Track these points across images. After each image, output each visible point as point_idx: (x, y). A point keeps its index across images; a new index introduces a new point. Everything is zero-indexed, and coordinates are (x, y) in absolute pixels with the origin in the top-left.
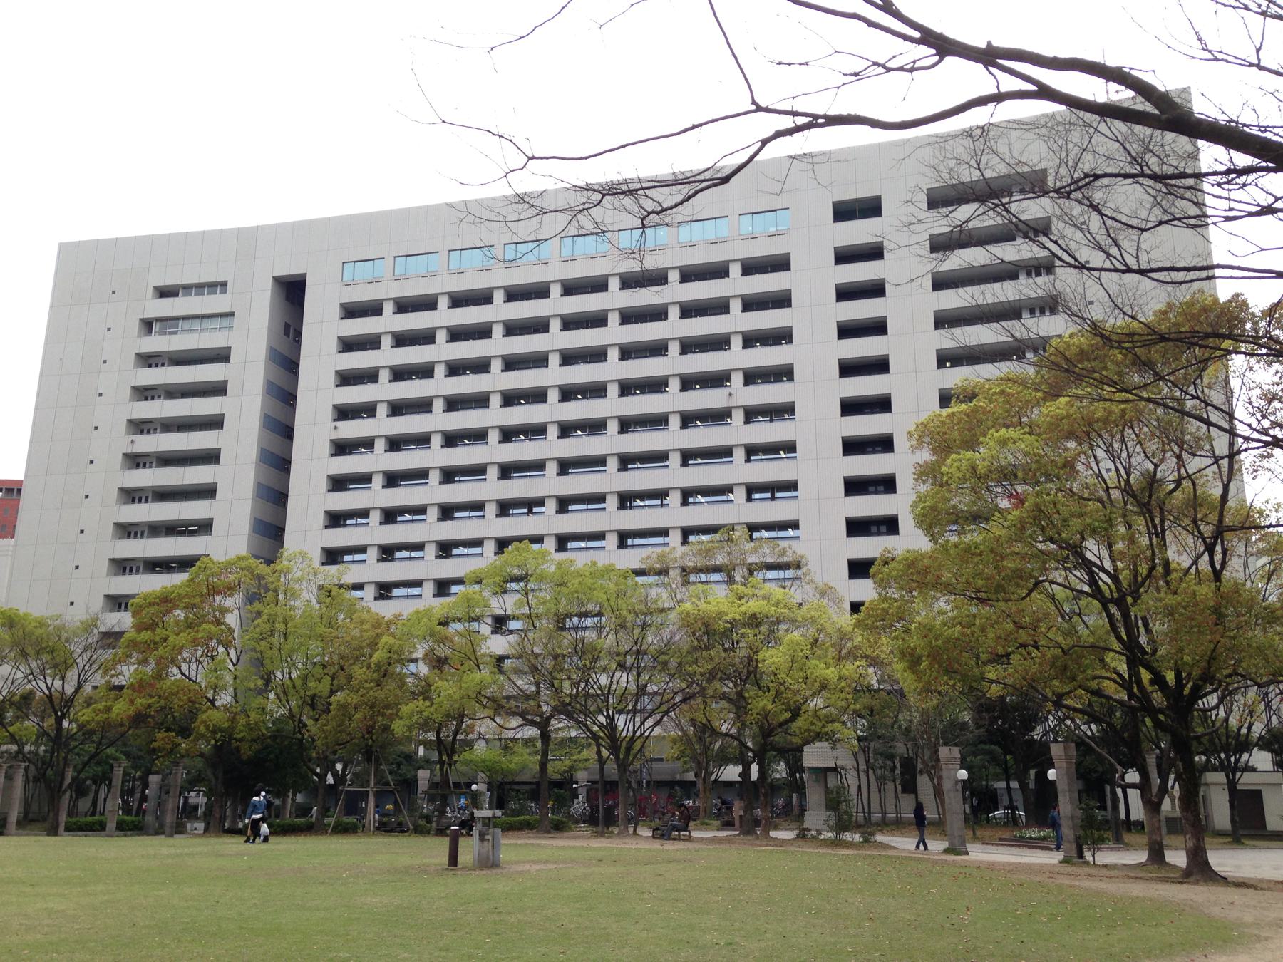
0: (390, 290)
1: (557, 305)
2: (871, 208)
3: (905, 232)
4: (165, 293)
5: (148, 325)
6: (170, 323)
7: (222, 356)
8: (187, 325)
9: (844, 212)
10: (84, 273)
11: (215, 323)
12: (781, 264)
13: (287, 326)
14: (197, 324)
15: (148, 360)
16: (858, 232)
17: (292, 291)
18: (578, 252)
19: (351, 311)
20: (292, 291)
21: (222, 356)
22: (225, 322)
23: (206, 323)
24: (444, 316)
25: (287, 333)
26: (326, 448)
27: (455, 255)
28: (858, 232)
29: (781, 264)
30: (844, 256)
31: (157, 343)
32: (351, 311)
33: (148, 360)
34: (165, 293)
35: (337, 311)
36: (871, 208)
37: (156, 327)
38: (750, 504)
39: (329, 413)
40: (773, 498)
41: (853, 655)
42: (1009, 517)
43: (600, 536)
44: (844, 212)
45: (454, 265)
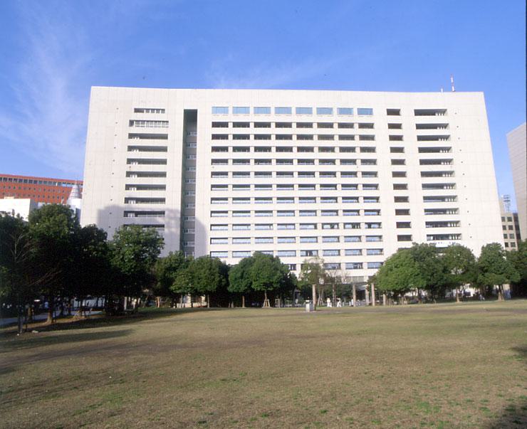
4: (137, 110)
5: (131, 123)
7: (165, 137)
15: (131, 136)
16: (394, 119)
21: (165, 137)
28: (394, 119)
31: (135, 130)
34: (137, 110)
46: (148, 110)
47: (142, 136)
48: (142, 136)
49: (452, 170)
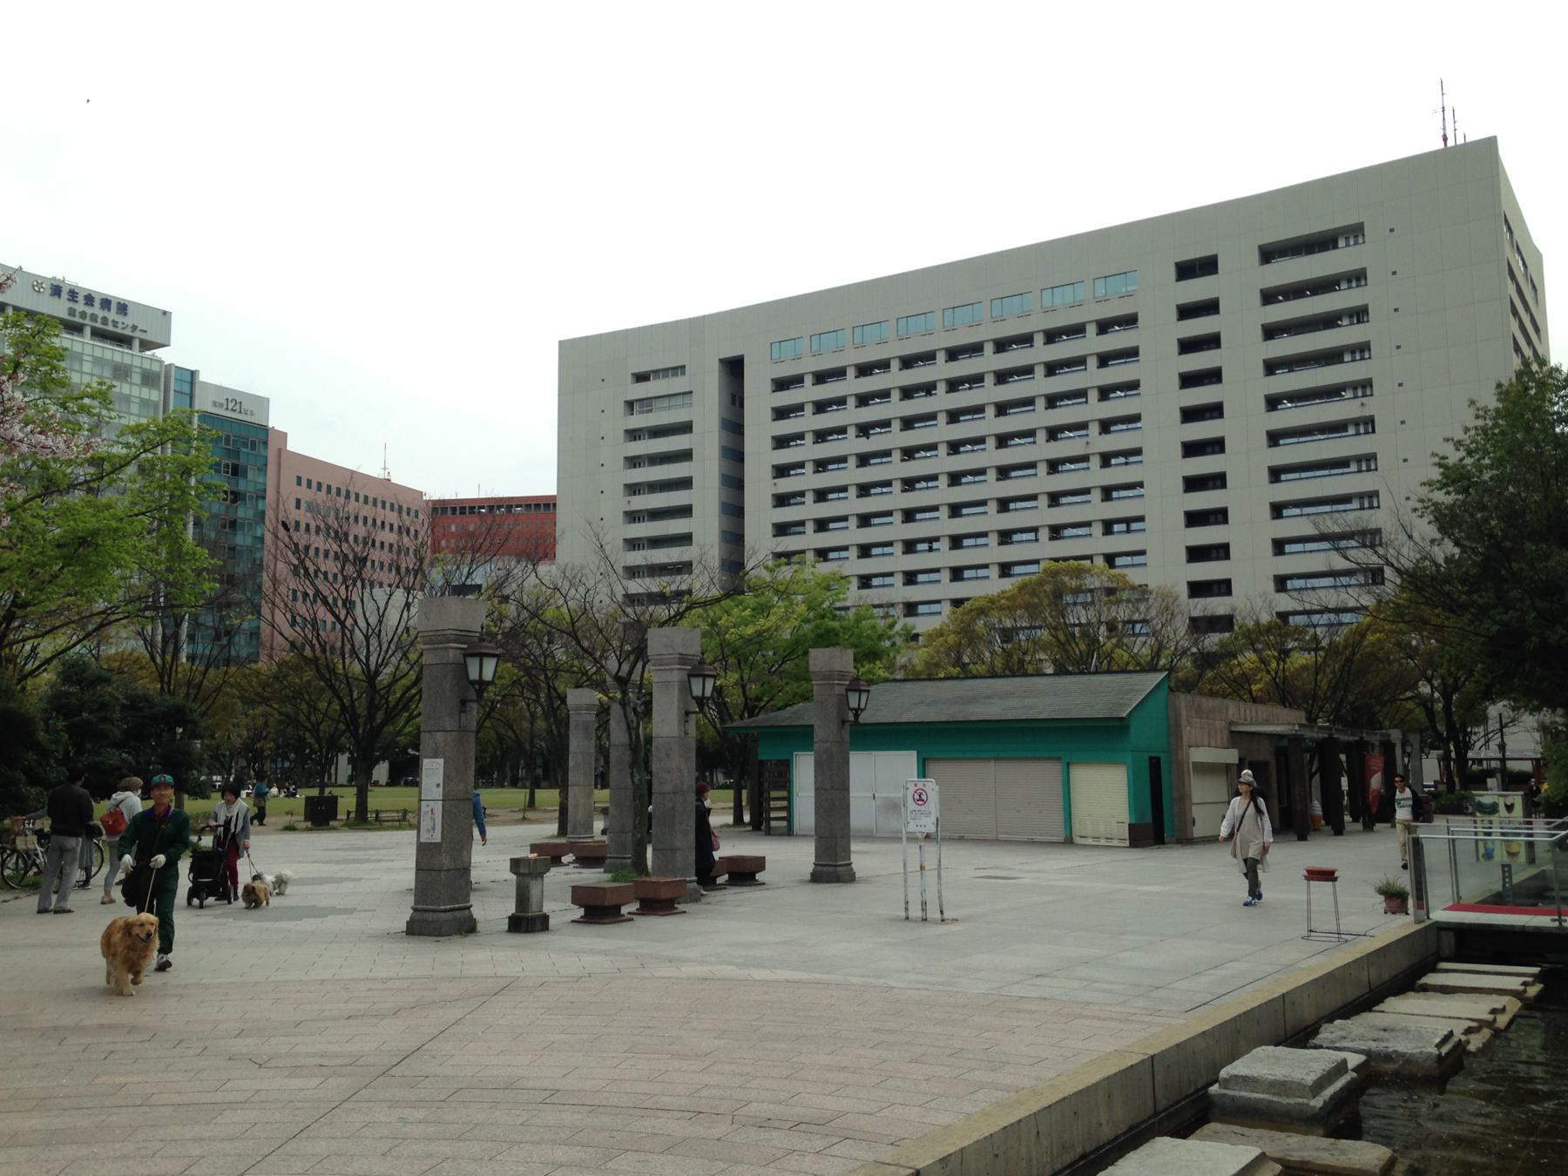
0: (809, 365)
1: (1041, 353)
2: (1208, 266)
3: (1239, 286)
4: (641, 378)
5: (630, 405)
6: (646, 403)
7: (686, 428)
8: (658, 403)
9: (1186, 271)
10: (581, 362)
11: (679, 400)
12: (1130, 321)
13: (733, 397)
14: (665, 403)
15: (634, 435)
16: (1198, 290)
17: (734, 368)
18: (1058, 301)
19: (781, 385)
20: (734, 368)
21: (686, 428)
22: (686, 399)
23: (673, 401)
24: (942, 370)
25: (733, 403)
26: (769, 501)
27: (1100, 283)
28: (1198, 290)
29: (1130, 321)
30: (1186, 312)
31: (639, 421)
32: (781, 385)
33: (634, 435)
34: (641, 378)
35: (769, 386)
36: (1208, 266)
37: (636, 407)
38: (1053, 443)
39: (769, 472)
40: (1128, 531)
41: (107, 892)
42: (923, 625)
43: (1032, 465)
44: (1186, 271)
45: (1047, 303)
46: (656, 373)
47: (657, 432)
48: (657, 432)
49: (1366, 413)
